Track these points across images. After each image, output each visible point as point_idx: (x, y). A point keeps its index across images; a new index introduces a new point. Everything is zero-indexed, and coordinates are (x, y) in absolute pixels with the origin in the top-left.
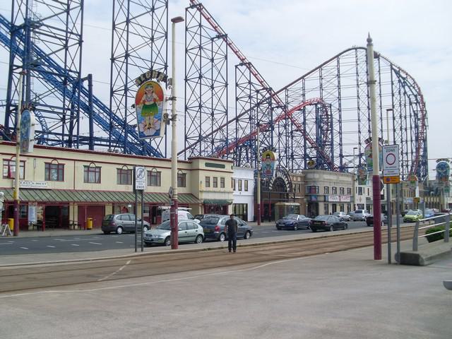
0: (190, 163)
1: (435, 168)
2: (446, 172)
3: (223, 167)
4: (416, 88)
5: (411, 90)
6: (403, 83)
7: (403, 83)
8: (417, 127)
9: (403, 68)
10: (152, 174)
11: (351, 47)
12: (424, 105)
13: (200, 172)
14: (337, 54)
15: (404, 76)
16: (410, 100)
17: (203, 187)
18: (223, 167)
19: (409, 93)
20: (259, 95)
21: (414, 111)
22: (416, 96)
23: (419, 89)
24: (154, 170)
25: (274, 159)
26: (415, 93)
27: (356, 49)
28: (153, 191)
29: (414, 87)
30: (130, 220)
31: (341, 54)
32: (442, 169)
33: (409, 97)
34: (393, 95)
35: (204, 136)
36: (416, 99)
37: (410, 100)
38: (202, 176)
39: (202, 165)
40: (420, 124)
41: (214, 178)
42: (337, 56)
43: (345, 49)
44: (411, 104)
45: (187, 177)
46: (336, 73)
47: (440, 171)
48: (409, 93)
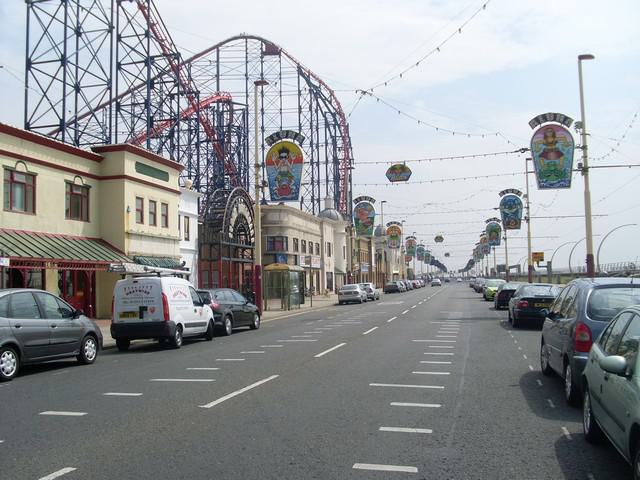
0: (99, 160)
1: (498, 206)
2: (517, 211)
3: (165, 176)
4: (334, 104)
5: (326, 106)
6: (316, 92)
7: (316, 92)
8: (336, 161)
9: (315, 73)
10: (17, 178)
11: (238, 34)
12: (347, 128)
13: (128, 185)
14: (216, 44)
15: (317, 84)
16: (326, 119)
17: (131, 223)
18: (165, 176)
19: (325, 109)
20: (152, 76)
21: (332, 137)
22: (334, 115)
23: (338, 104)
24: (21, 167)
25: (299, 160)
26: (333, 111)
27: (246, 37)
28: (17, 228)
29: (330, 102)
30: (43, 315)
31: (221, 44)
32: (510, 208)
33: (324, 116)
34: (300, 112)
35: (162, 51)
36: (335, 120)
37: (326, 119)
38: (131, 191)
39: (129, 167)
40: (341, 155)
41: (151, 201)
42: (217, 47)
43: (229, 37)
44: (327, 125)
45: (92, 193)
46: (216, 73)
47: (506, 211)
48: (325, 109)
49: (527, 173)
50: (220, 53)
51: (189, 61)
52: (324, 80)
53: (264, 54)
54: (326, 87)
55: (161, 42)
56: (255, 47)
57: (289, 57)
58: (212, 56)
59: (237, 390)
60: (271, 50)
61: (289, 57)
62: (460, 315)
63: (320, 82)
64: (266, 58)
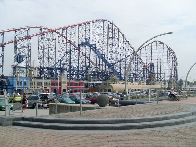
15: (171, 50)
56: (158, 43)
60: (162, 43)
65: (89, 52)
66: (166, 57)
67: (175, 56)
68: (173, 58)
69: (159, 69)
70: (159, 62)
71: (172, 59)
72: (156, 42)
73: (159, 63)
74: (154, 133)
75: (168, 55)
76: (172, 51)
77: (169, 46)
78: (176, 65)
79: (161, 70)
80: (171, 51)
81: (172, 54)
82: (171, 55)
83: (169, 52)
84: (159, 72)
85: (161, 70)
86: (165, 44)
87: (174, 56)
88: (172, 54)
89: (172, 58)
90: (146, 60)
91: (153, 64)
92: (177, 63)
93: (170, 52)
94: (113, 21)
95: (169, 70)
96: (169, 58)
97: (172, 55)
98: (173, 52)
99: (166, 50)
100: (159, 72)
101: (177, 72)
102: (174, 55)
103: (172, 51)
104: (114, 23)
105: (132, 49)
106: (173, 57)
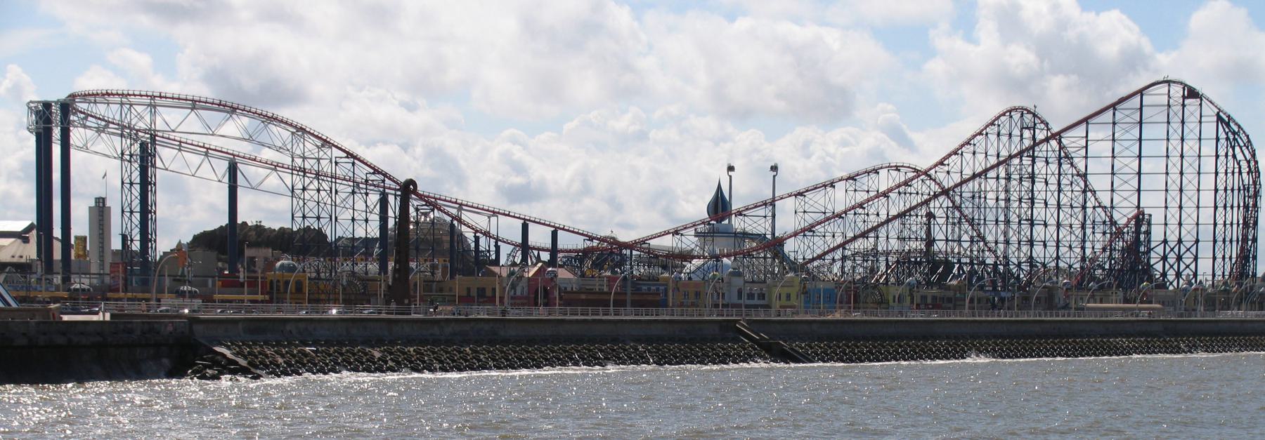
8: (1246, 207)
11: (1161, 79)
15: (1236, 129)
27: (1168, 82)
49: (1189, 232)
50: (1144, 97)
51: (1059, 133)
52: (1242, 125)
53: (1184, 97)
54: (1244, 132)
55: (1039, 118)
56: (1177, 91)
57: (1211, 102)
58: (1136, 101)
59: (1173, 358)
60: (1192, 93)
61: (1211, 102)
62: (1034, 255)
63: (1239, 127)
64: (1187, 101)
65: (1033, 251)
66: (1208, 165)
67: (1252, 164)
68: (1240, 173)
69: (1173, 221)
70: (1173, 204)
71: (1236, 175)
72: (1163, 89)
73: (1173, 211)
74: (1181, 395)
75: (1222, 152)
76: (1243, 136)
77: (1229, 109)
78: (1255, 205)
79: (1181, 190)
80: (1234, 133)
81: (1237, 149)
82: (1234, 156)
83: (1227, 139)
84: (1173, 238)
85: (1181, 190)
86: (1211, 98)
87: (1249, 162)
88: (1237, 149)
89: (1237, 170)
90: (1112, 190)
91: (1146, 217)
92: (1256, 194)
93: (1232, 143)
94: (1035, 107)
95: (1221, 193)
96: (1222, 170)
97: (1240, 156)
98: (1245, 139)
99: (1210, 129)
100: (1173, 238)
101: (1255, 240)
102: (1248, 157)
103: (1243, 136)
104: (1039, 111)
105: (1099, 210)
106: (1244, 164)
